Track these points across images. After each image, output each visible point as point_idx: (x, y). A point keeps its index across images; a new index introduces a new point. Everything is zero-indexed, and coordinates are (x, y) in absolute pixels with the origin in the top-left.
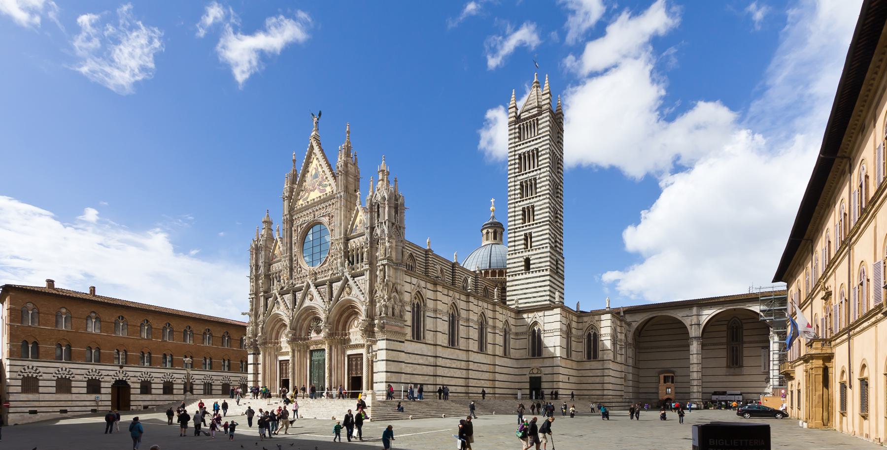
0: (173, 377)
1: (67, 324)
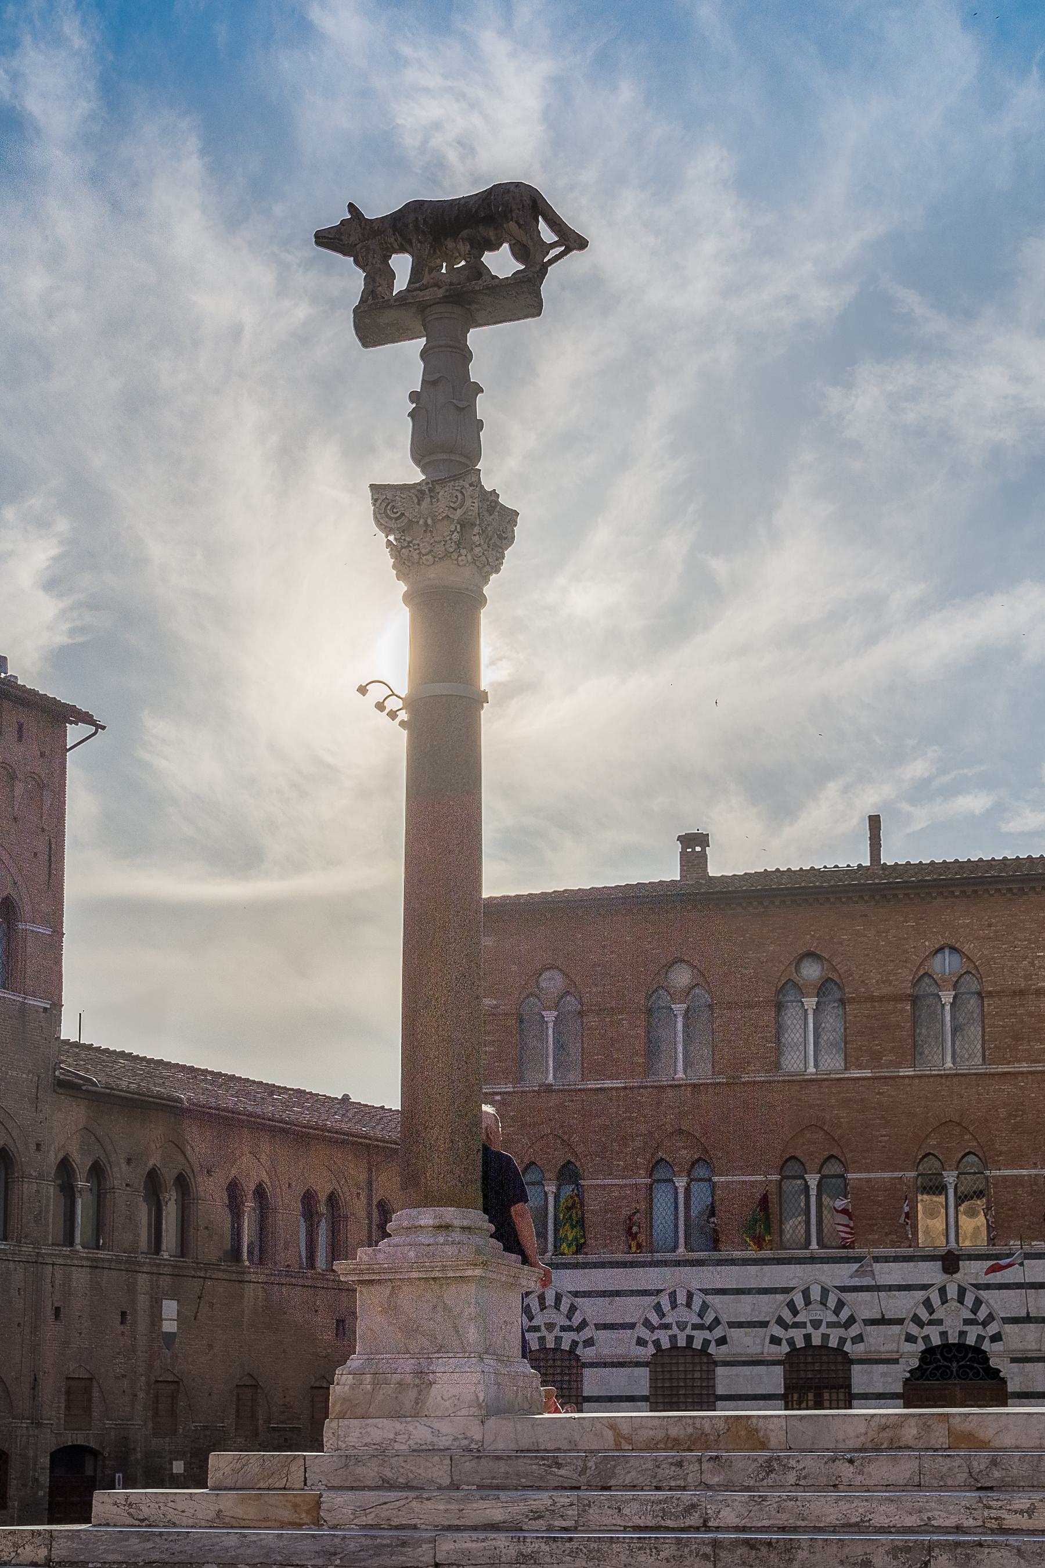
0: (983, 1313)
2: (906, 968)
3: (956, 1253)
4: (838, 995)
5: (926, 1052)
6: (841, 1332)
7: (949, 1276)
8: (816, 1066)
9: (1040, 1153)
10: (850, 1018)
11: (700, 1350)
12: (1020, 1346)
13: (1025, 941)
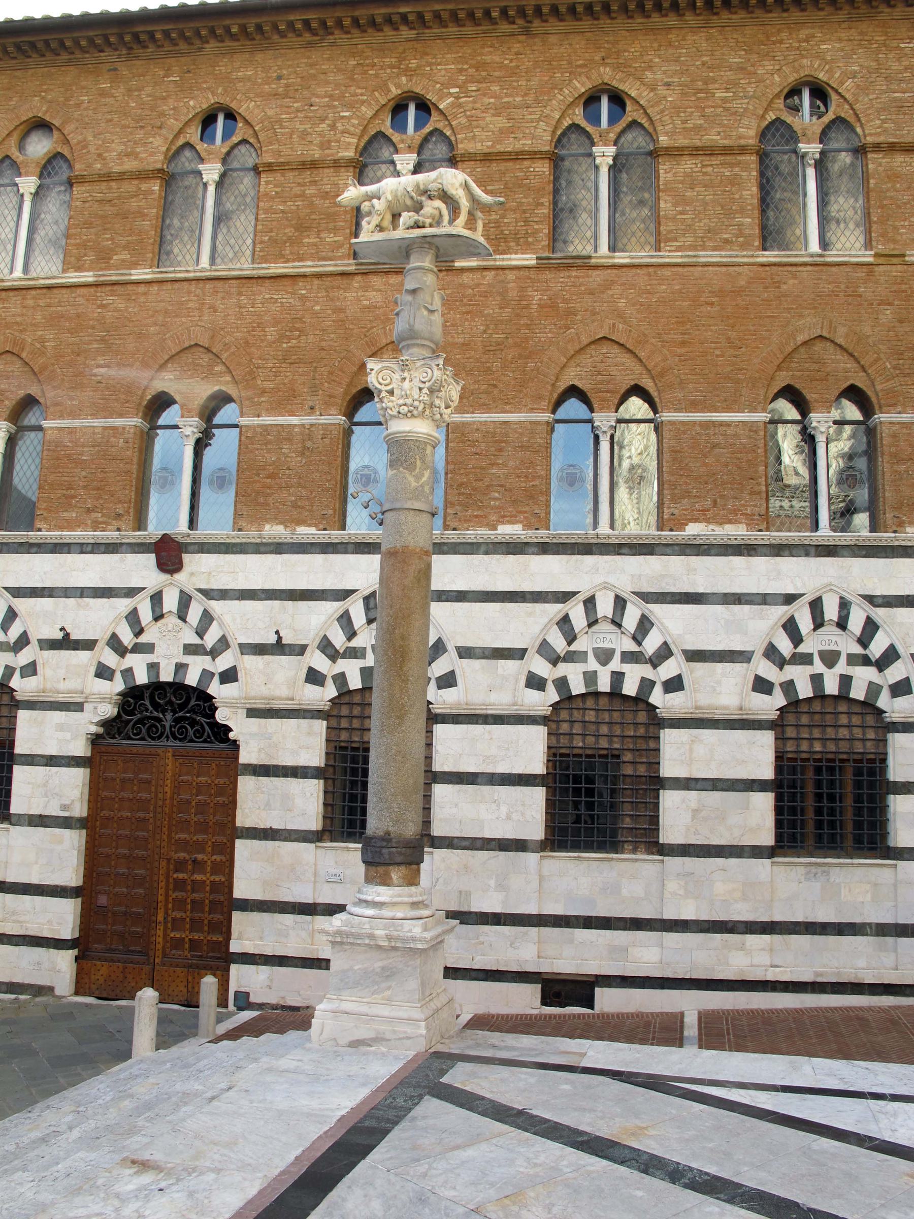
0: (651, 644)
1: (833, 209)
2: (160, 135)
3: (181, 540)
4: (65, 174)
5: (176, 251)
6: (646, 671)
7: (168, 576)
8: (26, 269)
9: (321, 392)
10: (78, 203)
11: (863, 703)
12: (265, 691)
13: (326, 97)
